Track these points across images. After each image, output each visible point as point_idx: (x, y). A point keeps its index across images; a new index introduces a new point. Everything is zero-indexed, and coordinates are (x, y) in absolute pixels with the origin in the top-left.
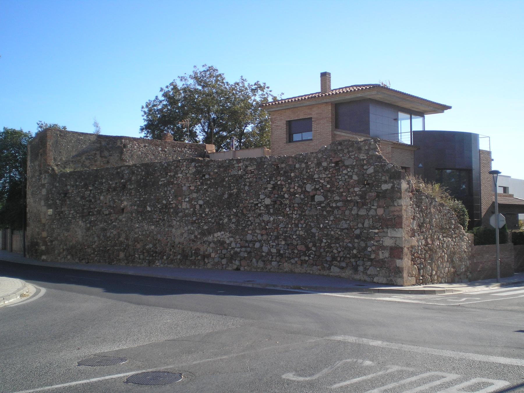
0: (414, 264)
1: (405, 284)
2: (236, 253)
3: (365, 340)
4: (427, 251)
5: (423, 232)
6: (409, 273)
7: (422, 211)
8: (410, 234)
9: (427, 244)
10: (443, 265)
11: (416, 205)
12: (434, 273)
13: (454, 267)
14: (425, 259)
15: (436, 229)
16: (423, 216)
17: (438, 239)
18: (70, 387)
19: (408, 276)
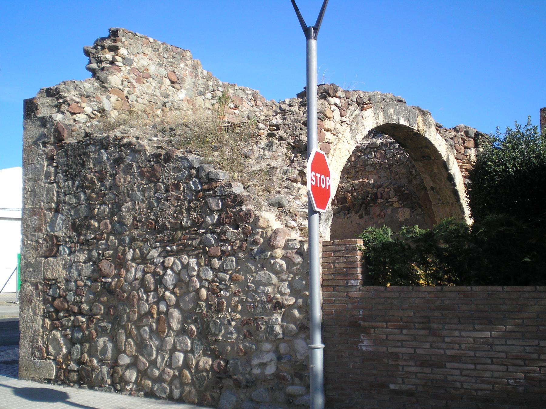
0: (54, 327)
1: (24, 373)
2: (376, 194)
3: (318, 314)
4: (98, 295)
5: (87, 243)
6: (34, 347)
7: (85, 185)
8: (43, 250)
9: (98, 275)
10: (163, 342)
11: (66, 173)
12: (125, 360)
13: (215, 356)
14: (90, 316)
15: (135, 233)
16: (88, 198)
17: (143, 259)
18: (471, 205)
19: (33, 354)
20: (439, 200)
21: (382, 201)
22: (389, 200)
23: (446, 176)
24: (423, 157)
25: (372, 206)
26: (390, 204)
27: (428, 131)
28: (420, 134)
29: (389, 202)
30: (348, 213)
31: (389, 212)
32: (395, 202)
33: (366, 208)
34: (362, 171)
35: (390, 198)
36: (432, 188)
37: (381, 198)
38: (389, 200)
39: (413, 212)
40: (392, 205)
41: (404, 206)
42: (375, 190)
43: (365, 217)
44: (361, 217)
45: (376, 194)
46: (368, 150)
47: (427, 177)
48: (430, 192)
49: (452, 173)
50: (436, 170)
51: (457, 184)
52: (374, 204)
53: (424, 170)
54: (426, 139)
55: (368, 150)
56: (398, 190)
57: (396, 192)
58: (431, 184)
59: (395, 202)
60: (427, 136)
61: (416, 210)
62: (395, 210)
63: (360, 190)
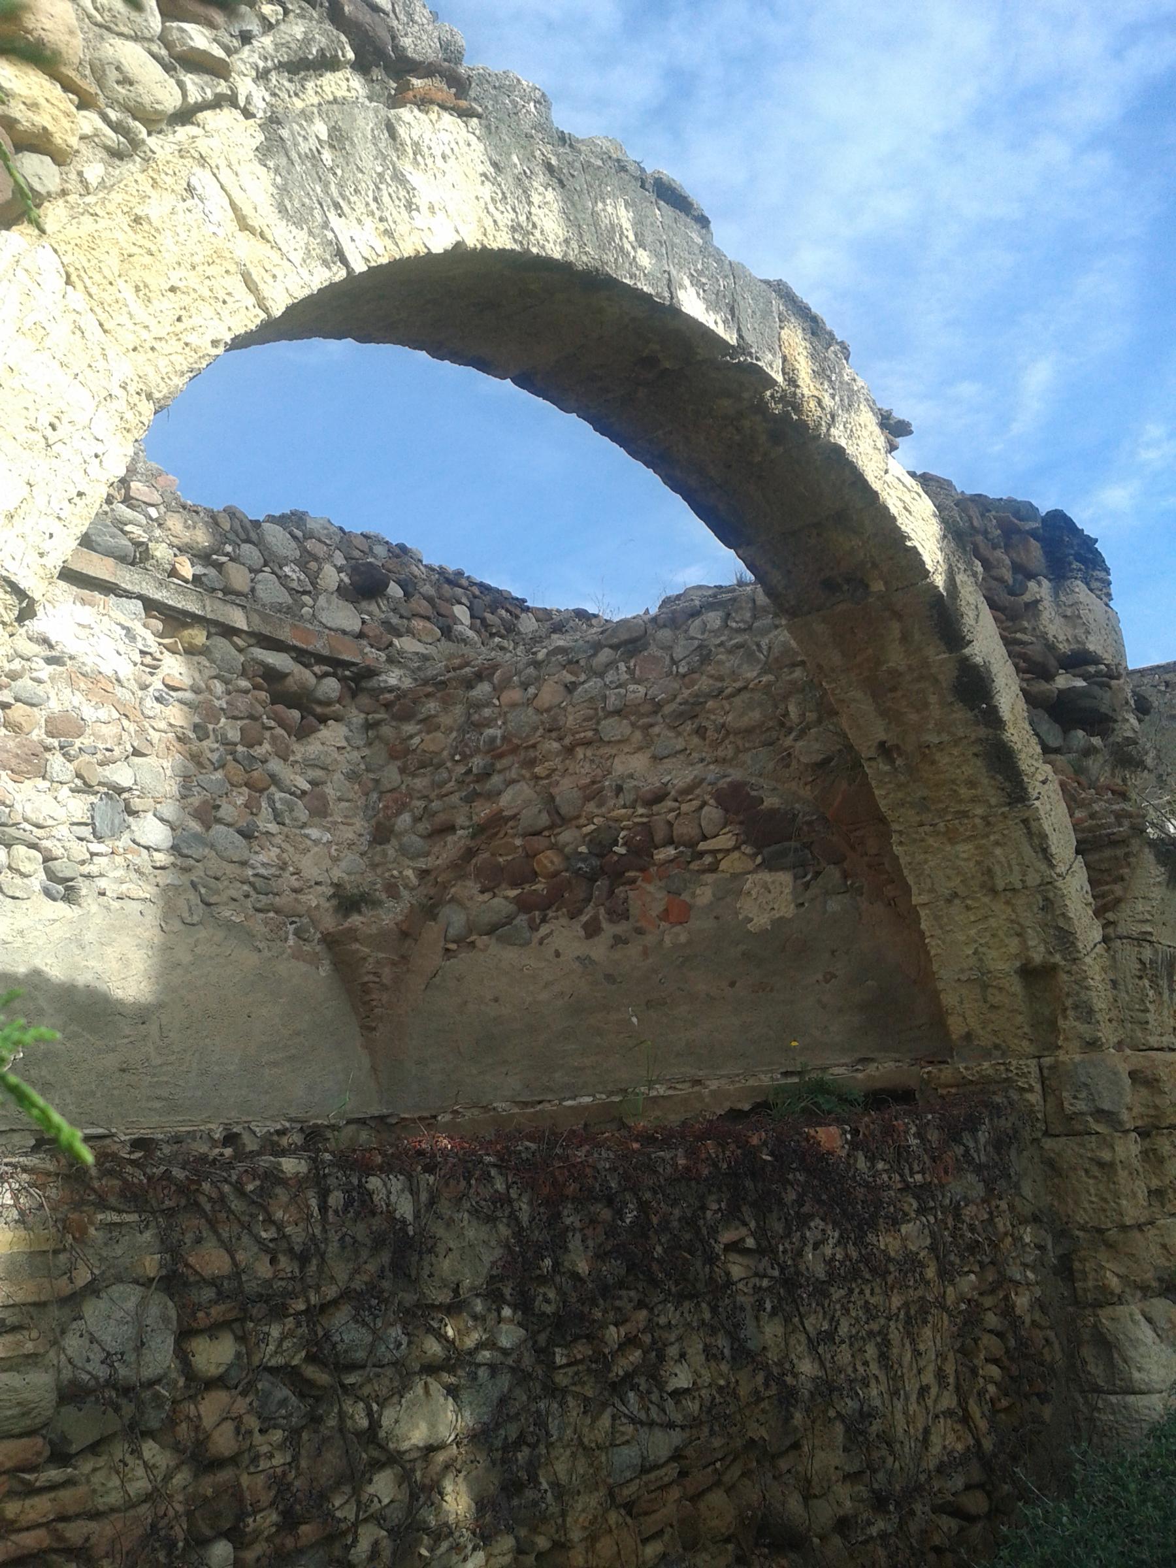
2: (647, 829)
20: (923, 805)
21: (671, 851)
22: (702, 846)
23: (947, 674)
24: (830, 586)
25: (633, 881)
26: (708, 859)
27: (843, 416)
28: (805, 425)
29: (701, 854)
30: (544, 920)
31: (704, 895)
32: (727, 851)
33: (611, 893)
34: (587, 743)
35: (705, 838)
36: (885, 750)
37: (670, 841)
38: (702, 846)
39: (807, 886)
40: (713, 868)
41: (769, 865)
42: (641, 811)
43: (610, 929)
44: (592, 930)
45: (647, 829)
46: (605, 655)
47: (859, 695)
48: (876, 769)
49: (979, 660)
50: (896, 658)
51: (1005, 712)
52: (643, 870)
53: (837, 659)
54: (839, 451)
55: (605, 655)
56: (736, 802)
57: (726, 810)
58: (880, 732)
59: (727, 851)
60: (838, 435)
61: (817, 874)
62: (732, 889)
63: (582, 821)
